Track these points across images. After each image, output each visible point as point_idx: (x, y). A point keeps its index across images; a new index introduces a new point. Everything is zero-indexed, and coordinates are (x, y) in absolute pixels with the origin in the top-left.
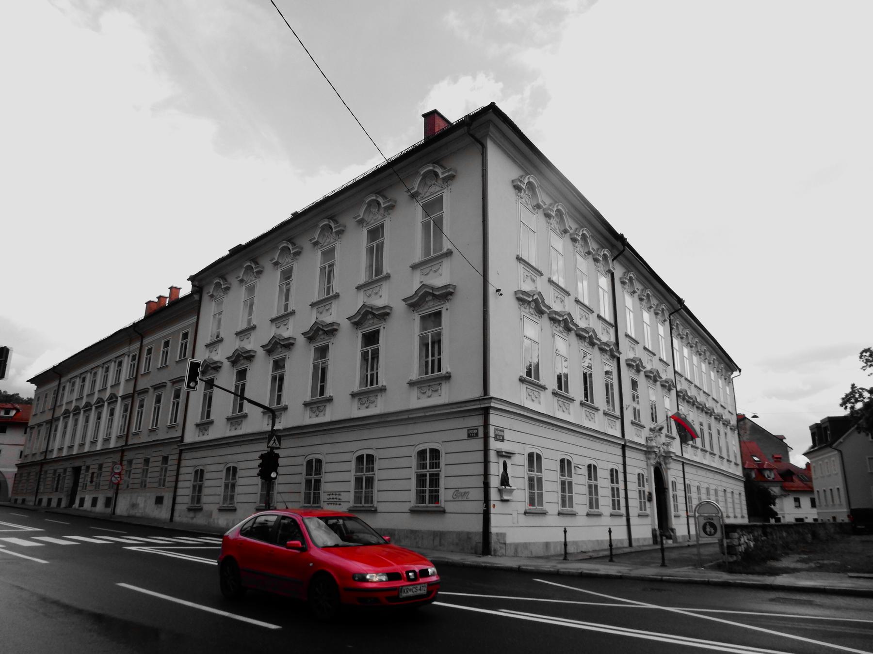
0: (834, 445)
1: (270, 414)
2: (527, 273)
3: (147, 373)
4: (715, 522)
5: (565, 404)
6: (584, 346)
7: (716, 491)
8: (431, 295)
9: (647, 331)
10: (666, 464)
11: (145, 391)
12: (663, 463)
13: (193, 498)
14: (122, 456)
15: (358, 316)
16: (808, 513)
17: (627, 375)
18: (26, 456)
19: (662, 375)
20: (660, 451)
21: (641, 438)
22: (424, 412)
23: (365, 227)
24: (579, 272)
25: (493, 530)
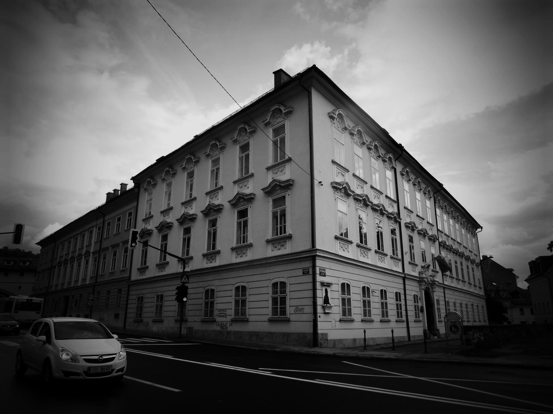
1: (182, 262)
2: (339, 171)
3: (108, 238)
7: (466, 305)
9: (419, 205)
10: (432, 288)
11: (107, 249)
12: (430, 288)
15: (235, 199)
16: (528, 317)
17: (406, 233)
19: (429, 232)
20: (428, 280)
21: (416, 272)
23: (238, 144)
24: (373, 169)
25: (320, 332)
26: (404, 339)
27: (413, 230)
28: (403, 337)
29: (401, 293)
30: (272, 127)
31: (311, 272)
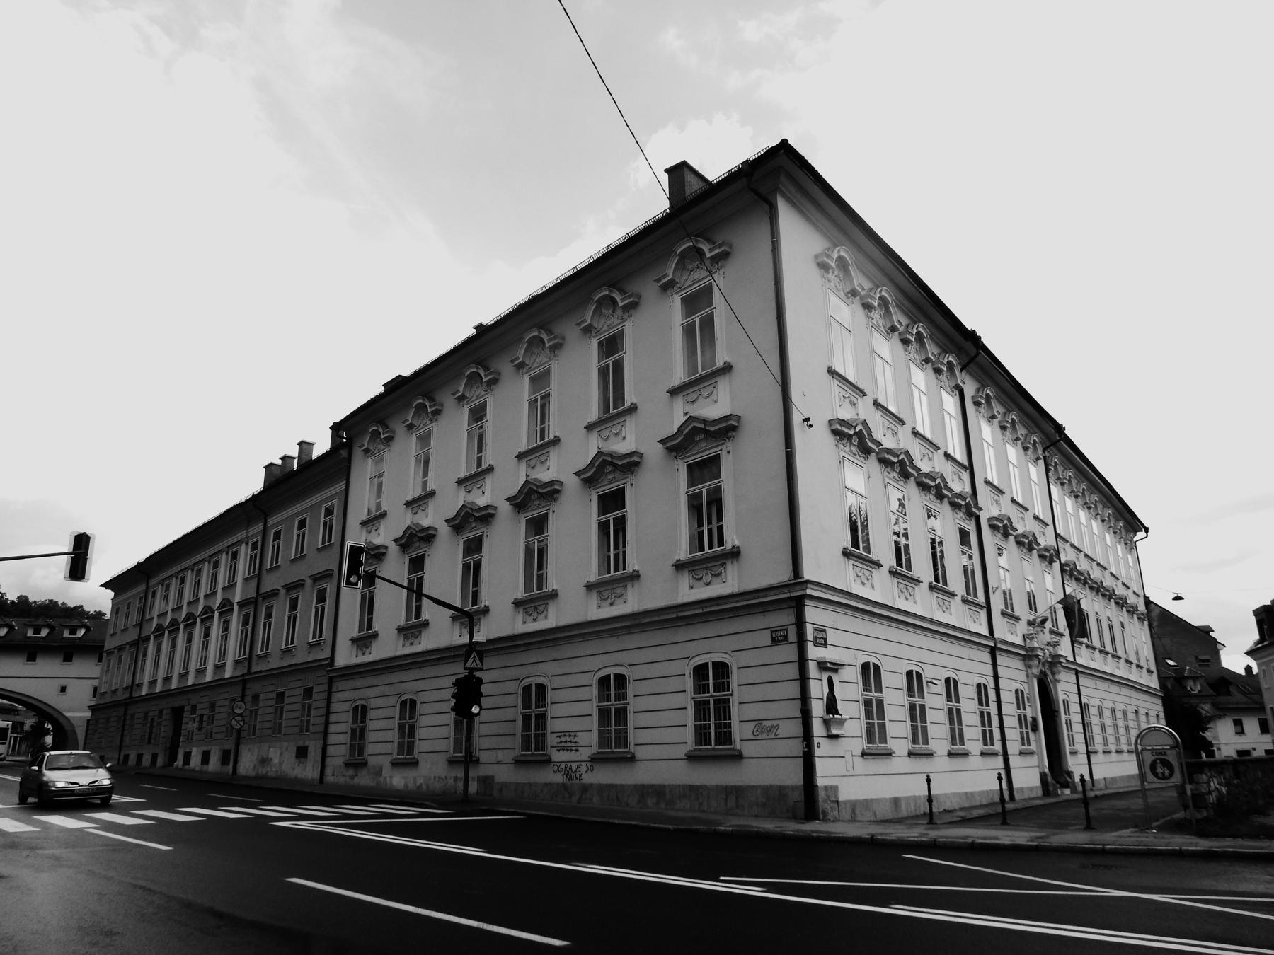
2: (843, 393)
5: (909, 588)
6: (929, 500)
8: (701, 432)
9: (1015, 475)
10: (1053, 674)
11: (274, 594)
12: (1049, 673)
13: (400, 745)
14: (244, 690)
15: (592, 468)
18: (102, 694)
21: (1017, 635)
22: (702, 608)
23: (594, 337)
25: (820, 782)
30: (529, 372)
31: (793, 637)
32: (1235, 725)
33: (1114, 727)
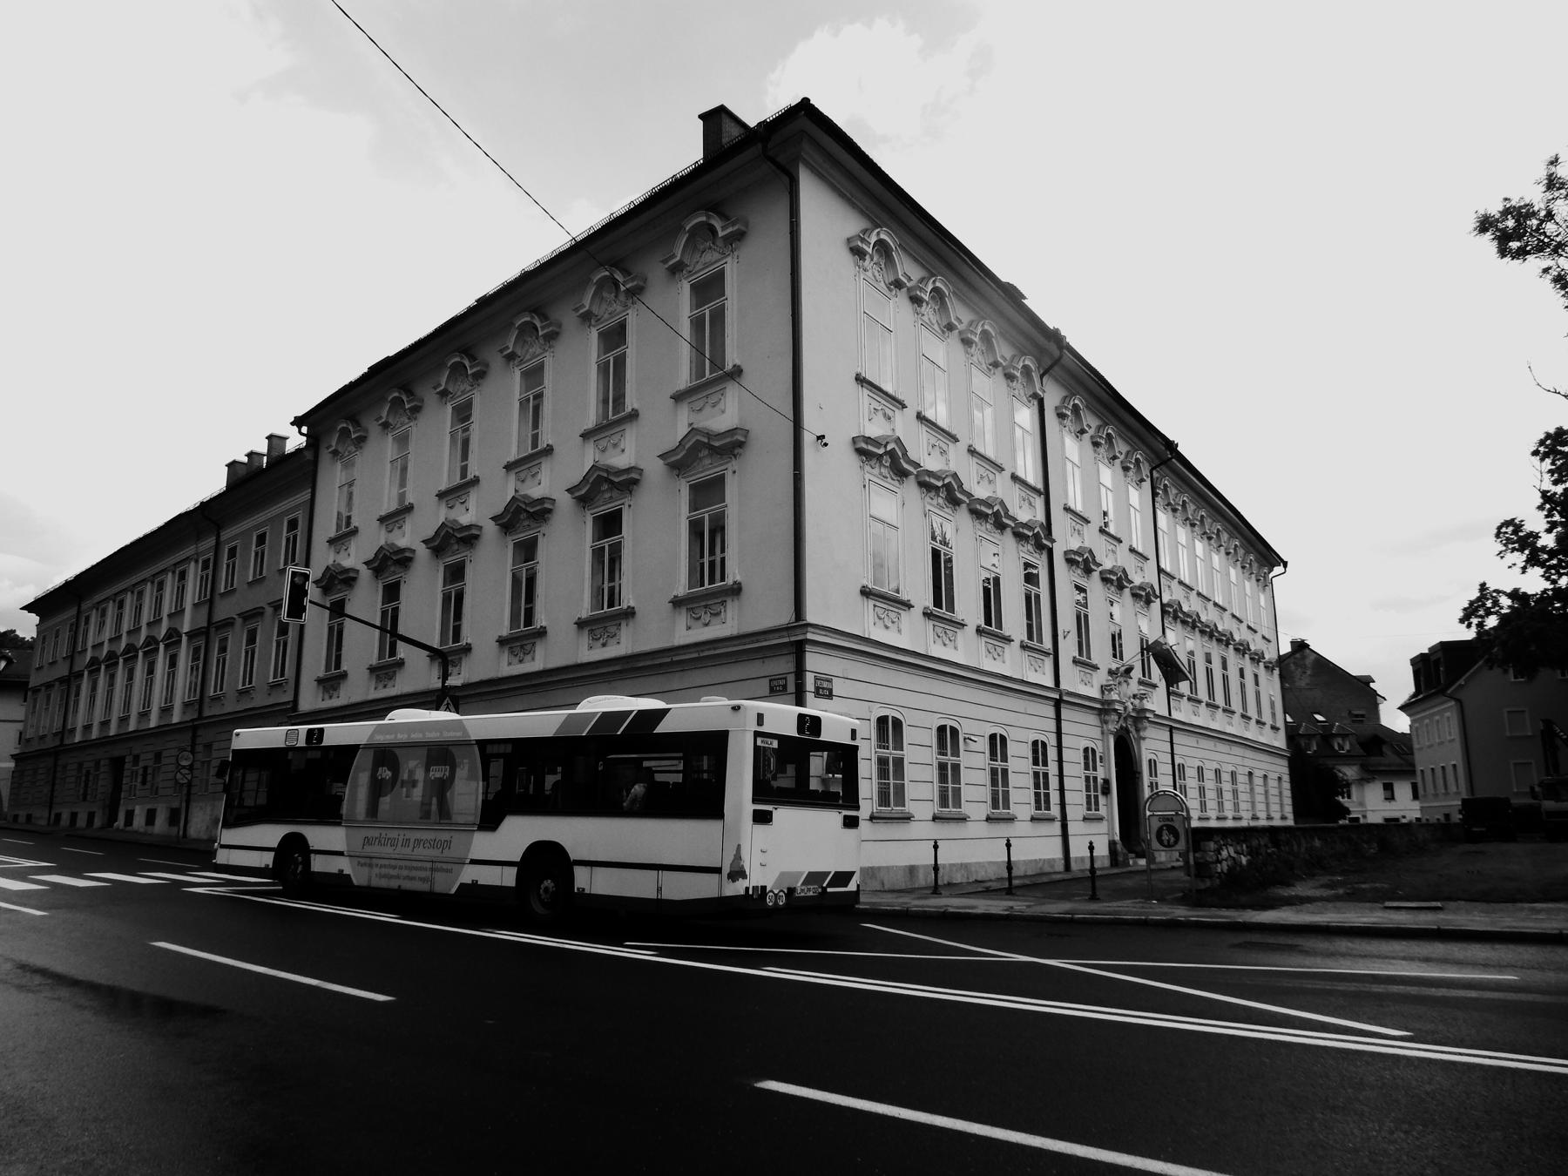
0: (1449, 692)
1: (440, 660)
3: (230, 593)
4: (1177, 825)
10: (1138, 730)
11: (228, 623)
12: (1132, 729)
16: (1405, 806)
18: (28, 741)
20: (1125, 708)
23: (594, 326)
26: (1052, 866)
27: (1088, 571)
28: (1051, 862)
29: (1047, 742)
30: (521, 365)
31: (791, 688)
32: (1385, 789)
33: (1217, 791)
